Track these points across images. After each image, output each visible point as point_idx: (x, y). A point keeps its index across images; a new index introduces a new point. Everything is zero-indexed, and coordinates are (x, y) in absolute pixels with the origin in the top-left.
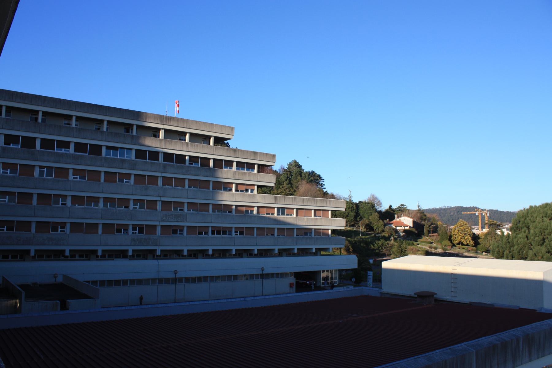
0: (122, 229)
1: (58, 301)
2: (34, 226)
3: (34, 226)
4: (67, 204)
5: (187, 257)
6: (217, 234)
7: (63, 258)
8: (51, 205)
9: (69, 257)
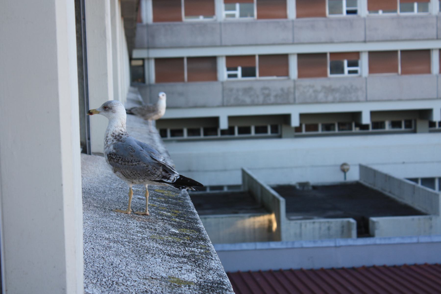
0: (346, 62)
1: (352, 220)
2: (293, 63)
3: (293, 63)
4: (359, 12)
5: (371, 130)
6: (261, 75)
7: (357, 130)
8: (324, 15)
9: (371, 127)
